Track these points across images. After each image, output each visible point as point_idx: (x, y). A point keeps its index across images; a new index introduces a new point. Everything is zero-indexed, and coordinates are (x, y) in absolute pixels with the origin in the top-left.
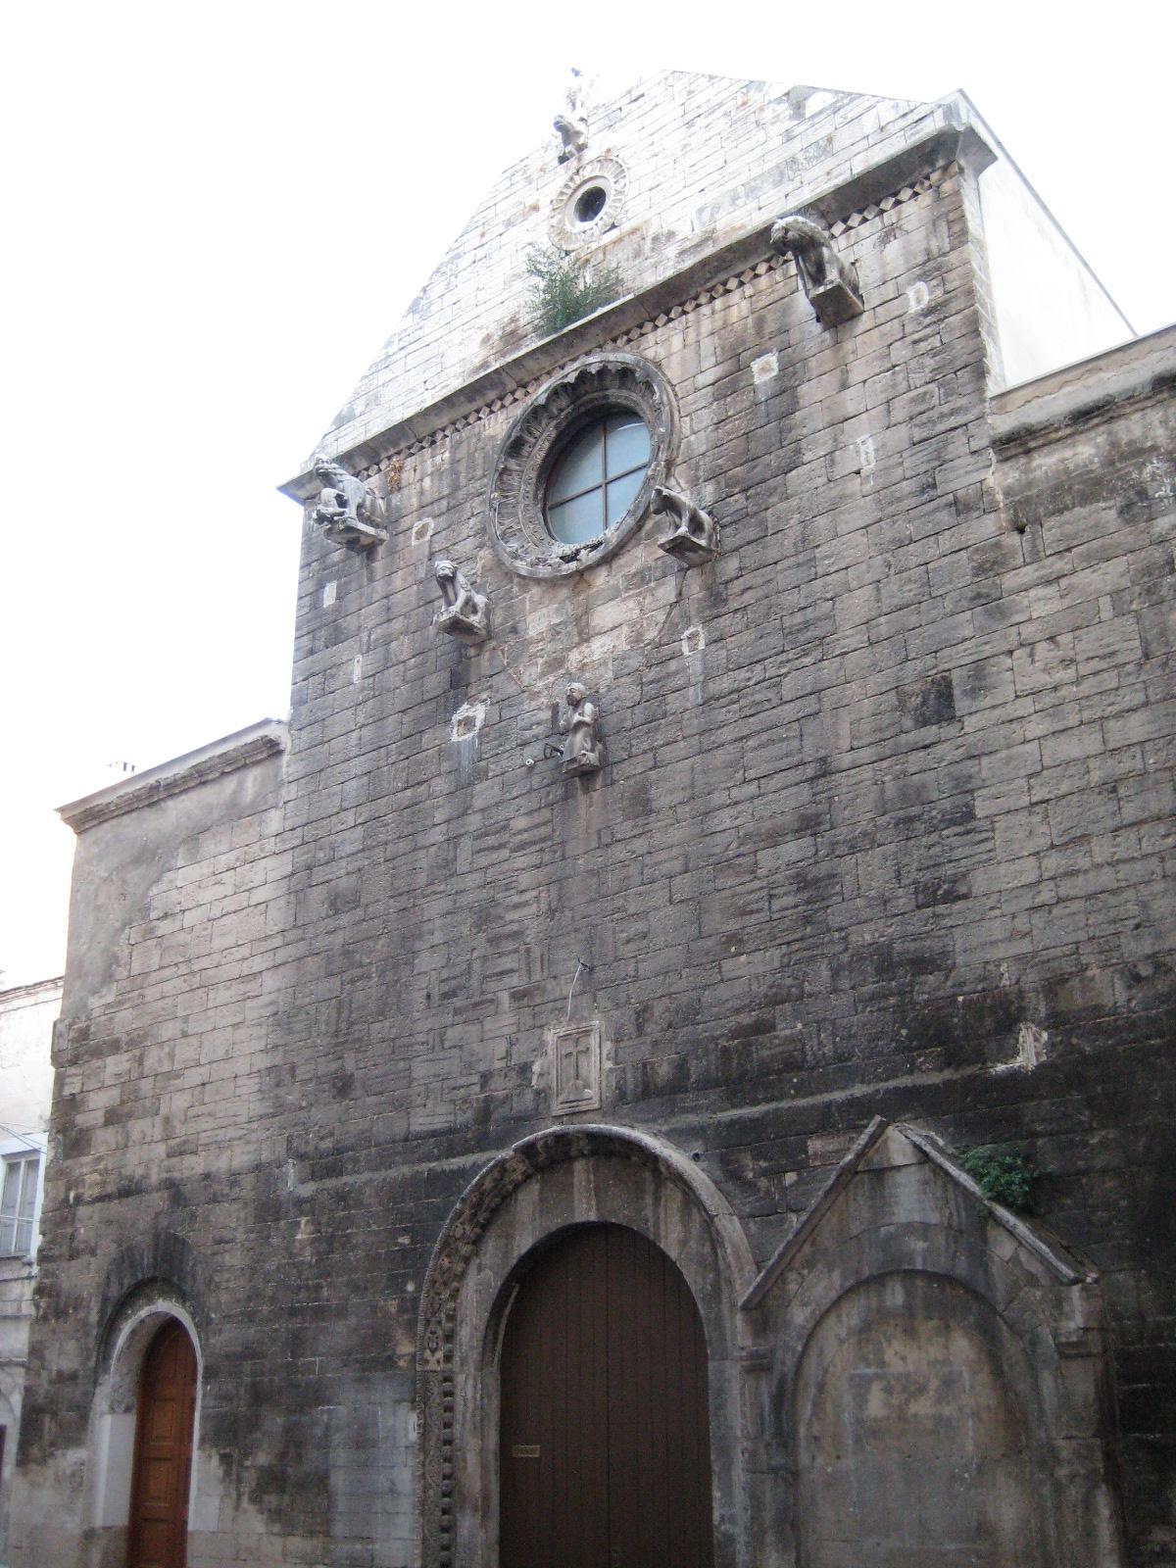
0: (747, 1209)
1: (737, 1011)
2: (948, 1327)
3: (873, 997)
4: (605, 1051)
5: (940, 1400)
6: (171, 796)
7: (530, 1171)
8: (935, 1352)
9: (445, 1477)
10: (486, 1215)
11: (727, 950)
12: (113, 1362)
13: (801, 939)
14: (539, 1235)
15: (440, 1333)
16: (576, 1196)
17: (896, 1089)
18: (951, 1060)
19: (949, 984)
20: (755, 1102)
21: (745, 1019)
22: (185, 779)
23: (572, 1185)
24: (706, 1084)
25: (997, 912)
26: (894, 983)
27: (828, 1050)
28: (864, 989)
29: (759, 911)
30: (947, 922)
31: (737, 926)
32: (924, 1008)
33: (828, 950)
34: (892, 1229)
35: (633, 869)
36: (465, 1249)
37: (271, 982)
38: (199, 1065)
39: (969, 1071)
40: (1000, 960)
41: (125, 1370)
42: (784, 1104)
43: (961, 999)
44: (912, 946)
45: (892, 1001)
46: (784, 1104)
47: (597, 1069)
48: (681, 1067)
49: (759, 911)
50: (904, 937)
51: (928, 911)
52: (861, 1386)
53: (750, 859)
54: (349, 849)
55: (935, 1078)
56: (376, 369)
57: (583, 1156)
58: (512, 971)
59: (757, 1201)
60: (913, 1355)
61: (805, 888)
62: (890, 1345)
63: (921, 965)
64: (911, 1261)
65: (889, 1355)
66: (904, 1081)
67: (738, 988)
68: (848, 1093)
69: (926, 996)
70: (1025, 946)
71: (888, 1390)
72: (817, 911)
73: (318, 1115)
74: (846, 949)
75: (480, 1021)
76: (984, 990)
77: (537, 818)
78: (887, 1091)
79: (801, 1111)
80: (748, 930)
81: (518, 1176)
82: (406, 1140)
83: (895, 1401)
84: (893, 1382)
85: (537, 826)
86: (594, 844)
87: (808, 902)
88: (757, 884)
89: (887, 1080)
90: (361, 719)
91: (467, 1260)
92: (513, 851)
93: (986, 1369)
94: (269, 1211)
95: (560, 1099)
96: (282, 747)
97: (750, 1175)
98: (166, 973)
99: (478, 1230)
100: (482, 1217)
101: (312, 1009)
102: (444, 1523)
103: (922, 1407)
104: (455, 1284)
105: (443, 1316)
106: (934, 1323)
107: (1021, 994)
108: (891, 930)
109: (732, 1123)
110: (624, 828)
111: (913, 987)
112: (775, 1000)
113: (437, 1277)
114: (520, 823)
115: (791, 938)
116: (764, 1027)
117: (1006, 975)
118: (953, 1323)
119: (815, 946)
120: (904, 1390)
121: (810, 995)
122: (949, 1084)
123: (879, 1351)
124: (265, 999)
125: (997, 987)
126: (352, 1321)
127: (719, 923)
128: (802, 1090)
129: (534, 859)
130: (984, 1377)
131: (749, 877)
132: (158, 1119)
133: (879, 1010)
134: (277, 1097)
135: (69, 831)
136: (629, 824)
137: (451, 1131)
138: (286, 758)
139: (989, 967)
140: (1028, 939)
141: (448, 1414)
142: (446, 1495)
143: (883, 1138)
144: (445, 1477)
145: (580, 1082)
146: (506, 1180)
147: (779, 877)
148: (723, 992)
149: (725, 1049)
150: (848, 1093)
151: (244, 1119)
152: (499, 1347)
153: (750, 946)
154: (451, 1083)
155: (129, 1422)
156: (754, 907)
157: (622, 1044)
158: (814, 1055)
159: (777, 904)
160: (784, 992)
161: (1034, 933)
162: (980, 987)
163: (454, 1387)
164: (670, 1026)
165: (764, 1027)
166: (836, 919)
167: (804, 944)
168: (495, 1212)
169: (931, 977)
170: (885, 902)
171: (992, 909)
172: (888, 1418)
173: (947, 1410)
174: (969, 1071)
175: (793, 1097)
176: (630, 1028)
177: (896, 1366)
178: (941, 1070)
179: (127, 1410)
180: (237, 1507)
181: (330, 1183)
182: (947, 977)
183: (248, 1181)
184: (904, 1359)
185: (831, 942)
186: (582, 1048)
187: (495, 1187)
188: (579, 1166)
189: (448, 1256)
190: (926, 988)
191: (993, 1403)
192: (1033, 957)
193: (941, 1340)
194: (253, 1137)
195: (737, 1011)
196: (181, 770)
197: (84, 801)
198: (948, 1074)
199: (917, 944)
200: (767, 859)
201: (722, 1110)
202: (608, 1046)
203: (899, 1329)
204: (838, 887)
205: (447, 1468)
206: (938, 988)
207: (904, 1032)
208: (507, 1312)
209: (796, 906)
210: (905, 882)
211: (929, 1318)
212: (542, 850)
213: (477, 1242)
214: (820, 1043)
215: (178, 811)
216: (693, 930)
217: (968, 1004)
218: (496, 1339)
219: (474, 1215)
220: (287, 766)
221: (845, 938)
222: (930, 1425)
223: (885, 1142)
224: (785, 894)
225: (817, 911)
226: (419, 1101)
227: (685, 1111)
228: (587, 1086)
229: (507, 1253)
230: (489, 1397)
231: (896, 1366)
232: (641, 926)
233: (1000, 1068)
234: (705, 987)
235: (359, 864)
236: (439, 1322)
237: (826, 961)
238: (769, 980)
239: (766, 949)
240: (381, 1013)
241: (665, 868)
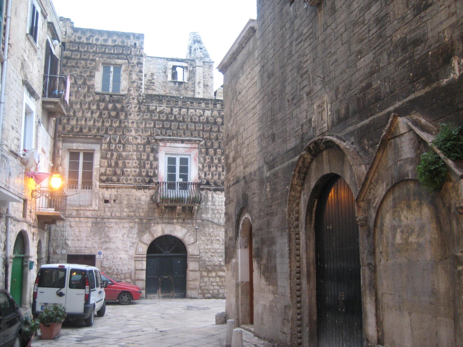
0: (367, 162)
1: (361, 82)
2: (421, 203)
3: (401, 62)
4: (328, 108)
5: (419, 236)
6: (237, 55)
7: (312, 157)
8: (417, 214)
9: (297, 267)
10: (303, 175)
11: (358, 58)
12: (240, 233)
13: (378, 45)
14: (316, 180)
15: (294, 218)
16: (324, 164)
17: (410, 100)
18: (428, 83)
19: (426, 48)
20: (367, 118)
21: (364, 84)
22: (238, 48)
23: (323, 161)
24: (355, 113)
25: (443, 7)
26: (407, 54)
27: (388, 90)
28: (398, 60)
29: (366, 38)
30: (425, 19)
31: (360, 47)
32: (418, 61)
33: (387, 47)
34: (401, 162)
35: (332, 36)
36: (299, 188)
37: (258, 107)
38: (247, 139)
39: (435, 85)
40: (444, 30)
41: (243, 236)
42: (375, 116)
43: (430, 53)
44: (413, 35)
45: (407, 62)
46: (375, 116)
47: (327, 116)
48: (347, 109)
49: (366, 38)
50: (410, 32)
51: (418, 17)
52: (394, 229)
53: (362, 18)
54: (271, 56)
55: (421, 93)
56: (134, 35)
57: (324, 149)
58: (306, 85)
59: (369, 158)
60: (410, 217)
61: (379, 23)
62: (402, 213)
63: (416, 42)
64: (407, 175)
65: (402, 217)
66: (412, 97)
67: (362, 72)
68: (394, 106)
69: (418, 56)
70: (453, 20)
71: (402, 232)
72: (382, 31)
73: (270, 148)
74: (392, 44)
75: (300, 106)
76: (438, 46)
77: (309, 26)
78: (407, 102)
79: (381, 117)
80: (363, 47)
81: (309, 160)
82: (287, 153)
83: (404, 237)
84: (404, 228)
85: (309, 30)
86: (323, 30)
87: (379, 29)
88: (365, 27)
89: (406, 97)
90: (270, 11)
91: (301, 192)
92: (304, 41)
93: (434, 221)
94: (262, 182)
95: (319, 129)
96: (255, 29)
97: (367, 147)
98: (240, 111)
99: (301, 181)
100: (302, 176)
101: (266, 113)
102: (298, 283)
103: (413, 239)
104: (297, 201)
105: (294, 212)
106: (416, 202)
107: (452, 43)
108: (406, 30)
109: (362, 127)
110: (329, 21)
111: (414, 53)
112: (371, 74)
113: (291, 199)
114: (305, 31)
115: (375, 46)
116: (369, 85)
117: (447, 36)
118: (423, 202)
119: (382, 47)
120: (407, 232)
121: (382, 68)
122: (427, 93)
123: (399, 216)
124: (258, 114)
125: (443, 43)
126: (279, 216)
127: (355, 47)
128: (381, 109)
129: (308, 43)
130: (434, 225)
131: (362, 25)
132: (241, 158)
133: (403, 67)
134: (262, 145)
135: (221, 73)
136: (331, 19)
137: (296, 147)
138: (257, 32)
139: (440, 35)
140: (455, 15)
141: (298, 246)
142: (297, 273)
143: (397, 122)
144: (297, 267)
145: (323, 122)
146: (306, 162)
147: (371, 22)
148: (357, 75)
149: (359, 98)
150: (394, 106)
151: (256, 154)
152: (313, 222)
153: (364, 53)
154: (295, 130)
155: (247, 251)
156: (364, 37)
157: (333, 104)
158: (384, 93)
159: (371, 33)
160: (374, 69)
161: (458, 11)
162: (437, 45)
163: (299, 236)
164: (344, 93)
165: (369, 85)
166: (388, 33)
167: (379, 47)
168: (306, 174)
169: (420, 47)
170: (404, 19)
171: (441, 6)
172: (402, 244)
173: (421, 240)
174: (435, 85)
175: (378, 113)
176: (334, 98)
177: (405, 222)
178: (424, 88)
179: (246, 247)
180: (260, 277)
181: (273, 171)
182: (425, 44)
183: (257, 173)
184: (407, 218)
185: (387, 43)
186: (323, 109)
187: (303, 165)
188: (325, 153)
189: (293, 191)
190: (418, 53)
191: (436, 236)
192: (457, 23)
193: (419, 209)
194: (258, 159)
195: (361, 82)
196: (237, 46)
197: (221, 64)
198: (427, 89)
199: (415, 33)
200: (368, 16)
201: (359, 123)
202: (329, 106)
203: (405, 205)
204: (388, 18)
205: (298, 264)
206: (422, 51)
207: (411, 75)
208: (314, 209)
209: (376, 32)
210: (410, 7)
211: (415, 200)
212: (311, 38)
213: (302, 185)
214: (385, 88)
215: (240, 58)
216: (348, 53)
217: (433, 54)
218: (311, 220)
219: (299, 176)
220: (258, 34)
221: (391, 40)
222: (415, 246)
223: (398, 124)
224: (373, 28)
225: (382, 31)
226: (288, 138)
227: (349, 125)
228: (324, 123)
229: (310, 188)
230: (310, 239)
231: (405, 222)
232: (335, 57)
233: (445, 82)
234: (352, 75)
235: (272, 61)
236: (293, 214)
237: (386, 52)
238: (370, 65)
239: (368, 54)
240: (279, 111)
241: (340, 32)
